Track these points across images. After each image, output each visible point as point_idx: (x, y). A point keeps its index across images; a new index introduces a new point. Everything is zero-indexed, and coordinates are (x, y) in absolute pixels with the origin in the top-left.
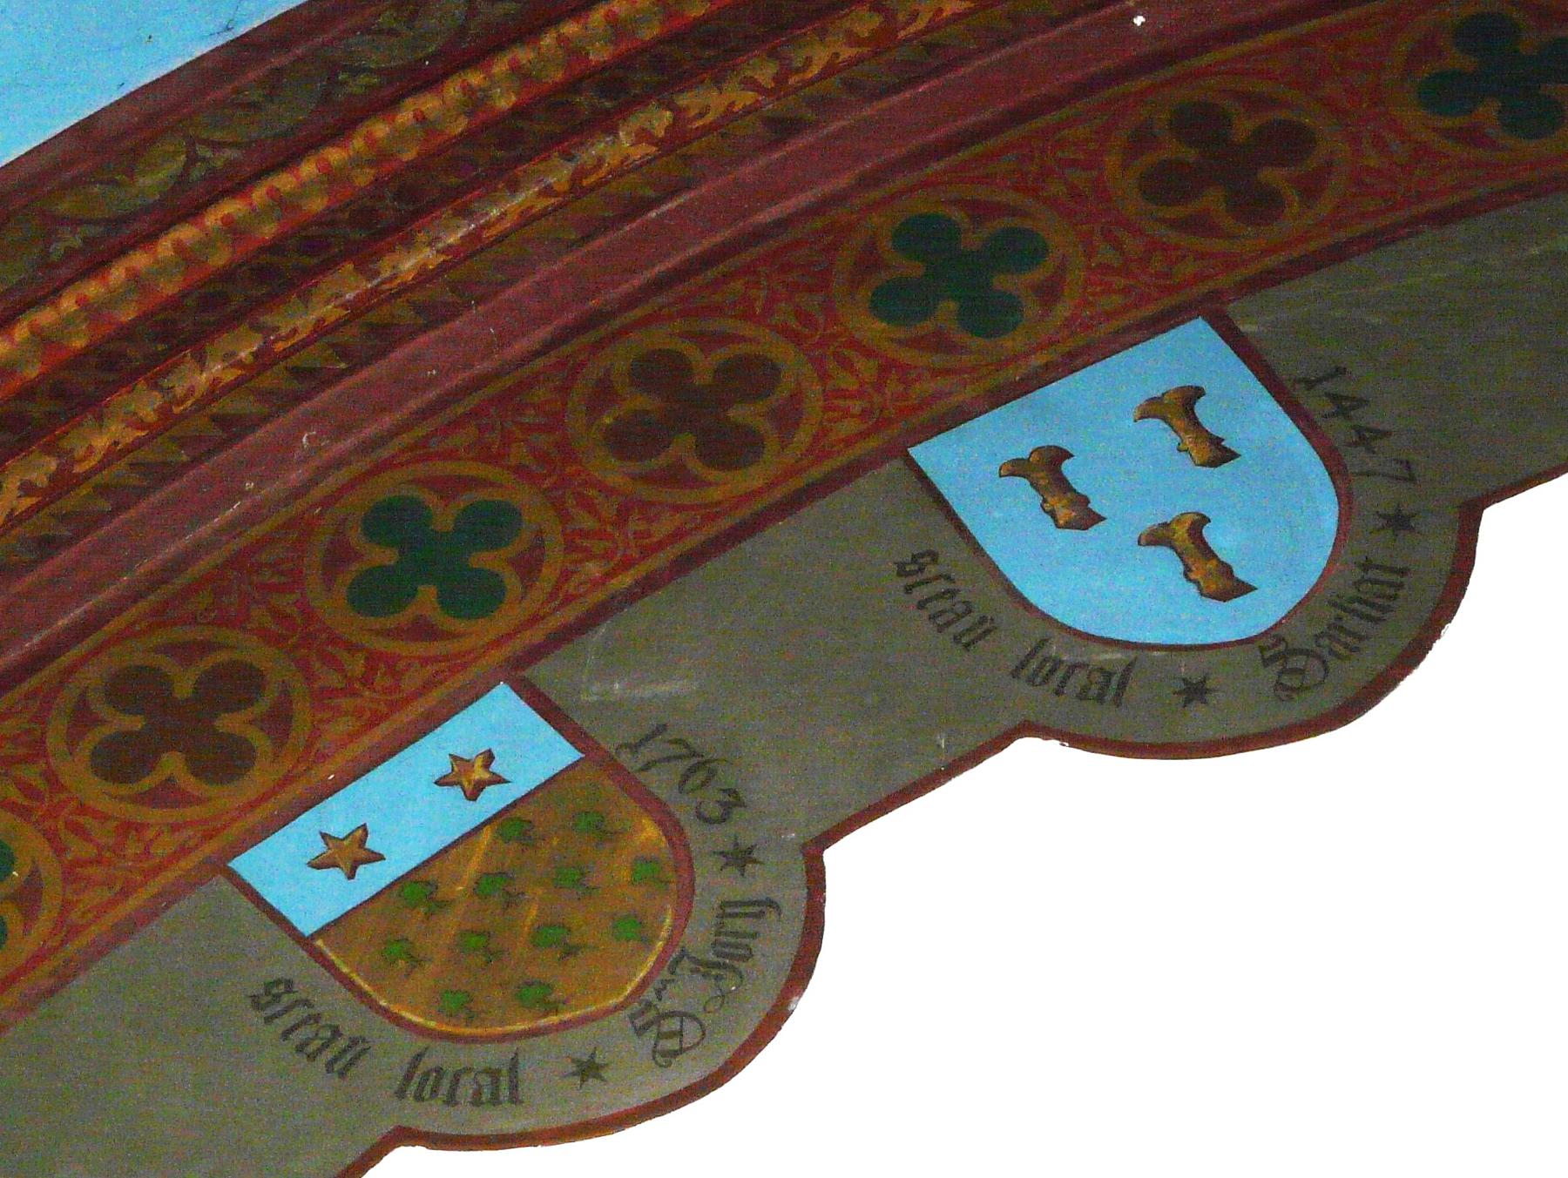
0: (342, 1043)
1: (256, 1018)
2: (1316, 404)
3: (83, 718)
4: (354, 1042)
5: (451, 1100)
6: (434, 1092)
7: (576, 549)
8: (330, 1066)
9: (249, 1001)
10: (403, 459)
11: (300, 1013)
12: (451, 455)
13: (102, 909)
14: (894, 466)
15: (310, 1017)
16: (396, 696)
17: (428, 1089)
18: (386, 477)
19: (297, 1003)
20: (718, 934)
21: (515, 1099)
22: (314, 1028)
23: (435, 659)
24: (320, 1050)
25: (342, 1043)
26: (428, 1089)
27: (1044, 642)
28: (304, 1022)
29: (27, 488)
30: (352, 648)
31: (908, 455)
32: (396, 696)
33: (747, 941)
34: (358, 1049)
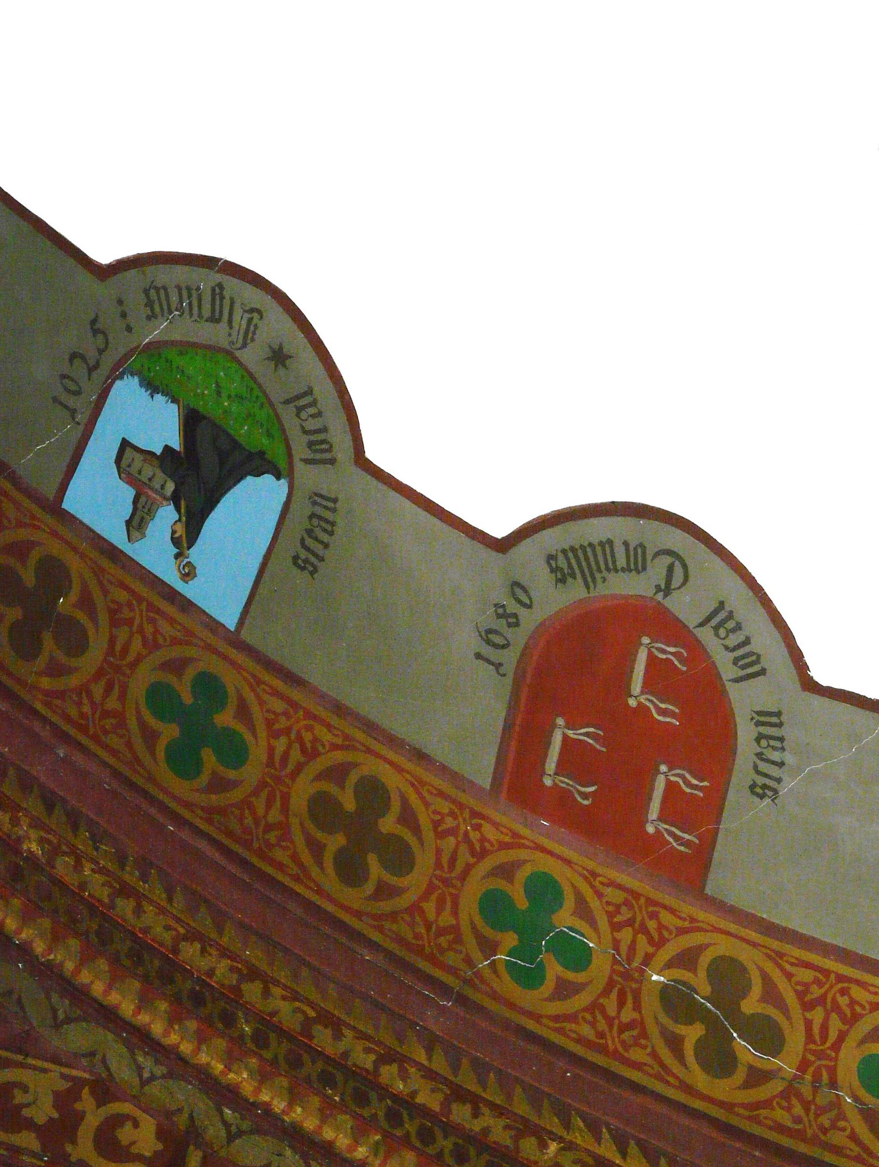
0: (319, 511)
1: (783, 790)
2: (82, 405)
3: (219, 784)
4: (315, 503)
5: (324, 430)
6: (323, 442)
7: (314, 749)
8: (780, 725)
9: (316, 576)
10: (312, 885)
11: (763, 767)
12: (295, 857)
13: (672, 911)
14: (245, 635)
15: (763, 760)
16: (630, 898)
17: (323, 446)
18: (327, 887)
19: (758, 772)
20: (630, 571)
21: (309, 392)
22: (765, 751)
23: (258, 696)
24: (327, 521)
25: (762, 729)
26: (323, 446)
27: (737, 680)
28: (767, 761)
29: (476, 1114)
30: (271, 750)
31: (236, 631)
32: (821, 977)
33: (631, 549)
34: (316, 498)
